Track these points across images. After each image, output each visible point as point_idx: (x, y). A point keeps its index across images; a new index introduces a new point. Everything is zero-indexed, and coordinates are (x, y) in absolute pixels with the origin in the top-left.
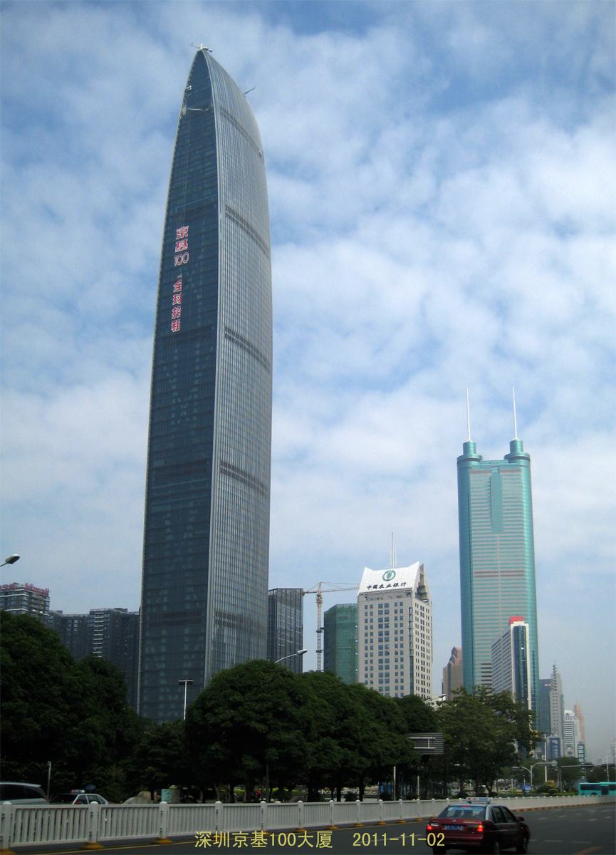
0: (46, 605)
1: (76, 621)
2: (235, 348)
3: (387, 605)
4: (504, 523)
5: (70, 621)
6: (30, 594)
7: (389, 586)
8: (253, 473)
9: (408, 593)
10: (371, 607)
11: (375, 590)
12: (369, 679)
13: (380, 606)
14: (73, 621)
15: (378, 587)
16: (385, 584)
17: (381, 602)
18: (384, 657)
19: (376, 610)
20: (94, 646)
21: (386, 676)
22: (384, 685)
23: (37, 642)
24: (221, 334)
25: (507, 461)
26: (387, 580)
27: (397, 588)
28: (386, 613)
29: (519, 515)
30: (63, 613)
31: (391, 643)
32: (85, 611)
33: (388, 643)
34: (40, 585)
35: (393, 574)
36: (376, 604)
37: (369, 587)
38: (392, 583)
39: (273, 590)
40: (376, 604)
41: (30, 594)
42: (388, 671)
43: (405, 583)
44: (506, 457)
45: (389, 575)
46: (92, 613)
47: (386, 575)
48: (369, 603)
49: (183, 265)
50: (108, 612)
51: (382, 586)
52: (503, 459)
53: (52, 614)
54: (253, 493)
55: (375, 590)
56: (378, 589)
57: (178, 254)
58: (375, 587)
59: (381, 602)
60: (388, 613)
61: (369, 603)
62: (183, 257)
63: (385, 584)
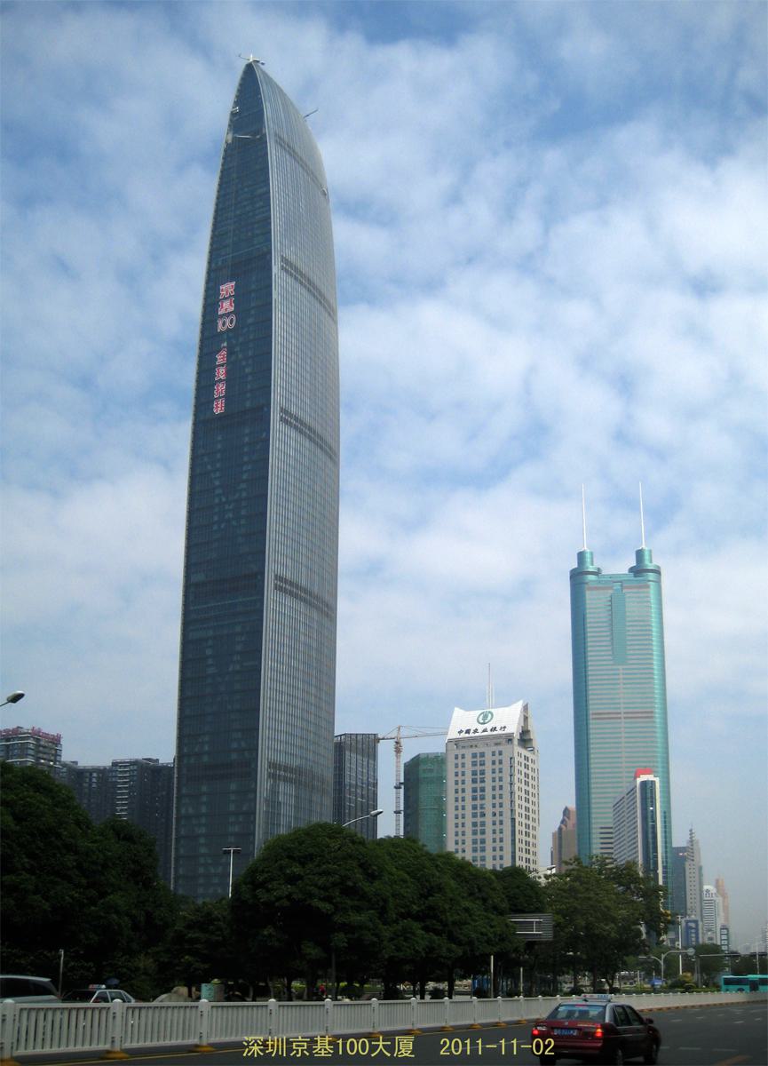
0: (57, 754)
1: (95, 775)
2: (293, 433)
3: (482, 755)
4: (629, 652)
5: (88, 774)
6: (38, 740)
7: (485, 731)
8: (316, 590)
9: (509, 739)
10: (463, 757)
11: (467, 735)
12: (460, 847)
13: (474, 756)
14: (91, 774)
15: (472, 731)
16: (481, 728)
17: (475, 750)
18: (479, 820)
19: (468, 760)
20: (118, 805)
21: (481, 843)
22: (479, 854)
23: (46, 801)
24: (275, 416)
25: (632, 574)
26: (482, 724)
27: (495, 733)
28: (481, 765)
29: (647, 642)
30: (79, 765)
31: (488, 802)
32: (106, 762)
33: (483, 802)
34: (50, 729)
35: (490, 715)
36: (468, 753)
37: (460, 732)
38: (489, 726)
39: (341, 736)
40: (468, 753)
41: (38, 740)
42: (483, 837)
43: (505, 727)
44: (631, 570)
45: (485, 717)
46: (115, 764)
47: (481, 717)
48: (460, 752)
49: (228, 330)
50: (135, 763)
51: (476, 731)
52: (627, 572)
53: (65, 765)
54: (315, 615)
55: (467, 735)
56: (471, 735)
57: (222, 316)
58: (468, 732)
59: (475, 750)
60: (484, 764)
61: (460, 752)
62: (228, 321)
63: (481, 728)
